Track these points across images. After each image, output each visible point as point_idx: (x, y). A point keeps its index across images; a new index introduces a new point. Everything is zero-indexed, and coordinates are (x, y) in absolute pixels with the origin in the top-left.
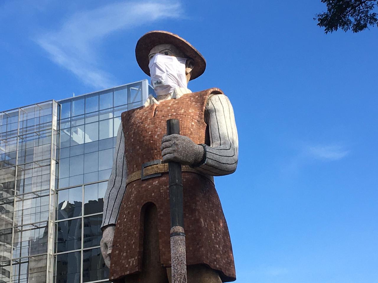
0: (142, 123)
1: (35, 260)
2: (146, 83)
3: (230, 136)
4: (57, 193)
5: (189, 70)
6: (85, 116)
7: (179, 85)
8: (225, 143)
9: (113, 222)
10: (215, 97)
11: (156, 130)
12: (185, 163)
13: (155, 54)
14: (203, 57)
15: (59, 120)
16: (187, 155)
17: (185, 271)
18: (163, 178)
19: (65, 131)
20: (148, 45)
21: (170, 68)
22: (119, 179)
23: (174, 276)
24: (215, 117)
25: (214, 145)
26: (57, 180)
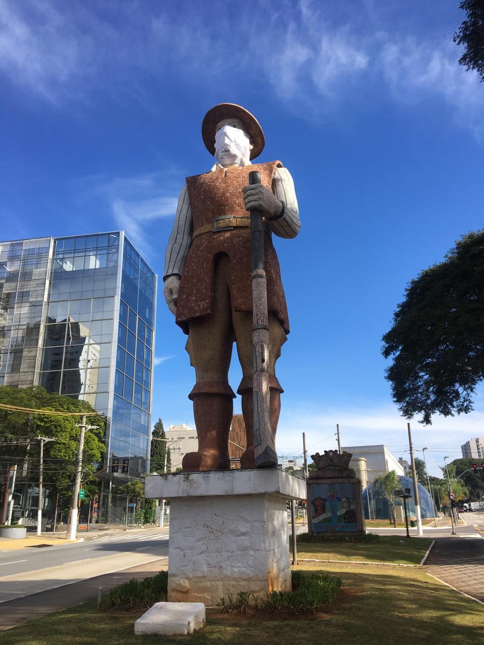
0: (213, 182)
1: (28, 351)
2: (122, 233)
4: (48, 305)
9: (176, 271)
10: (280, 169)
11: (228, 188)
13: (223, 125)
15: (54, 252)
16: (270, 205)
21: (235, 139)
22: (180, 236)
23: (257, 315)
24: (281, 185)
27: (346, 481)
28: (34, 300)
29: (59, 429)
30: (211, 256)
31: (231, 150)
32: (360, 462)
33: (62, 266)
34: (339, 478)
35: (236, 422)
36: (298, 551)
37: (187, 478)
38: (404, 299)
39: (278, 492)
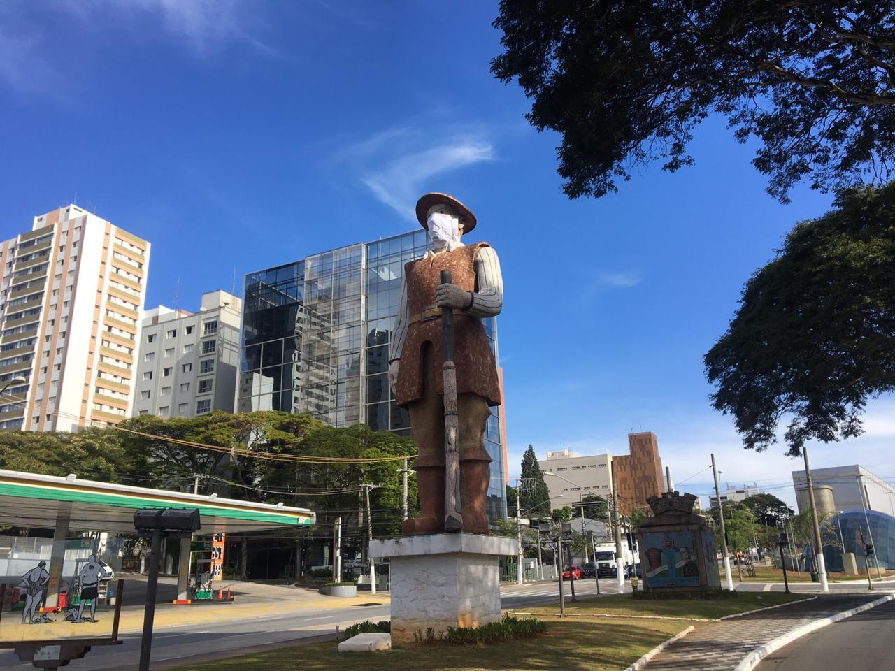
3: (496, 284)
5: (462, 226)
6: (389, 256)
7: (453, 239)
8: (490, 290)
9: (398, 356)
10: (483, 249)
12: (456, 308)
13: (432, 212)
14: (473, 214)
15: (367, 260)
17: (455, 398)
18: (439, 320)
19: (373, 270)
20: (427, 205)
21: (445, 225)
22: (403, 320)
25: (481, 292)
26: (367, 312)
27: (684, 528)
28: (351, 320)
29: (386, 474)
30: (419, 345)
31: (439, 236)
32: (822, 491)
33: (378, 275)
34: (677, 524)
35: (636, 443)
36: (565, 607)
37: (398, 542)
38: (739, 307)
39: (461, 552)
